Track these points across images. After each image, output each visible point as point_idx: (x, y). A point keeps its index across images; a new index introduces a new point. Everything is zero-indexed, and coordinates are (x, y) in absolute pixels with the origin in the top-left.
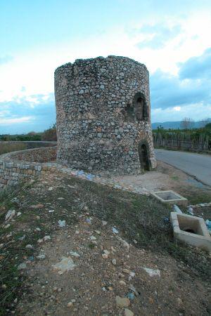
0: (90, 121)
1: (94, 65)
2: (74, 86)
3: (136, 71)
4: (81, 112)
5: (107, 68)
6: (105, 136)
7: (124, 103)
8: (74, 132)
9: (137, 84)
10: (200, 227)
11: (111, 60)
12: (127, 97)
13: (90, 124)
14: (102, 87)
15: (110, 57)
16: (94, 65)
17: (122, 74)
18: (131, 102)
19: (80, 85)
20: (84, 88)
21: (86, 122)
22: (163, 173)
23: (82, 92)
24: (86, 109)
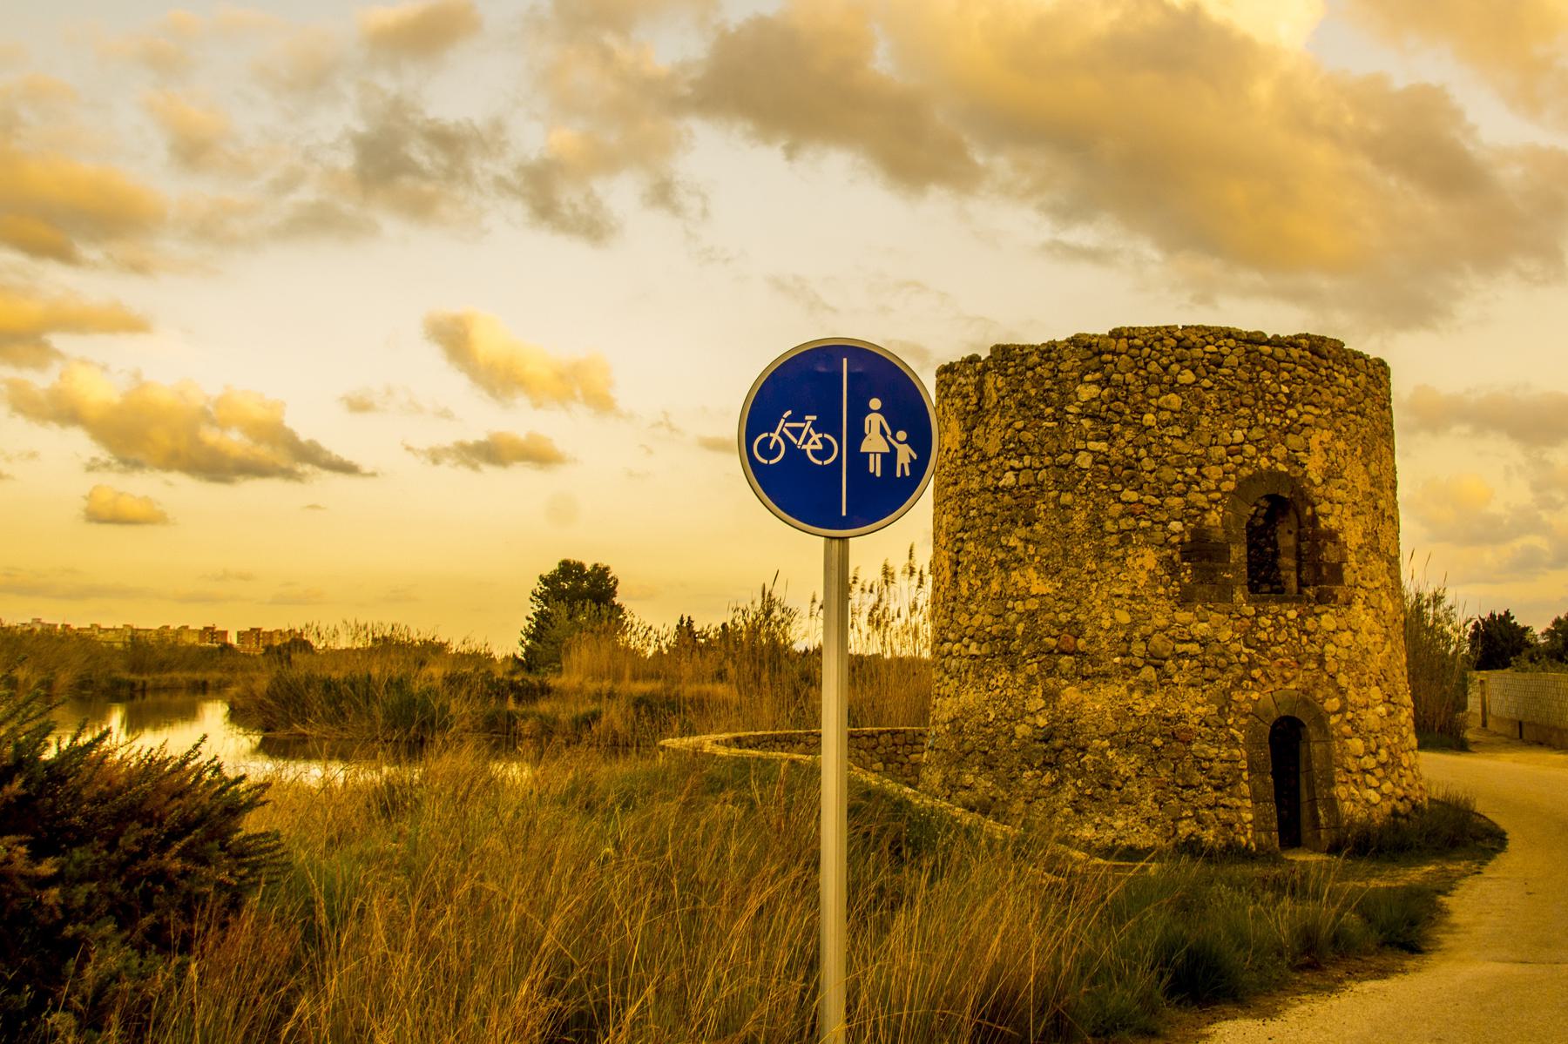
0: (1033, 605)
1: (1055, 372)
2: (984, 458)
3: (1375, 375)
4: (1001, 564)
5: (1105, 382)
6: (386, 861)
7: (1176, 526)
8: (973, 649)
9: (1257, 433)
10: (1246, 1016)
11: (1122, 345)
12: (1191, 497)
13: (1032, 615)
14: (1084, 461)
15: (1116, 334)
16: (1055, 372)
17: (1175, 400)
18: (1213, 518)
19: (1004, 451)
20: (1016, 463)
21: (1019, 606)
22: (888, 931)
23: (1009, 479)
24: (1020, 551)
